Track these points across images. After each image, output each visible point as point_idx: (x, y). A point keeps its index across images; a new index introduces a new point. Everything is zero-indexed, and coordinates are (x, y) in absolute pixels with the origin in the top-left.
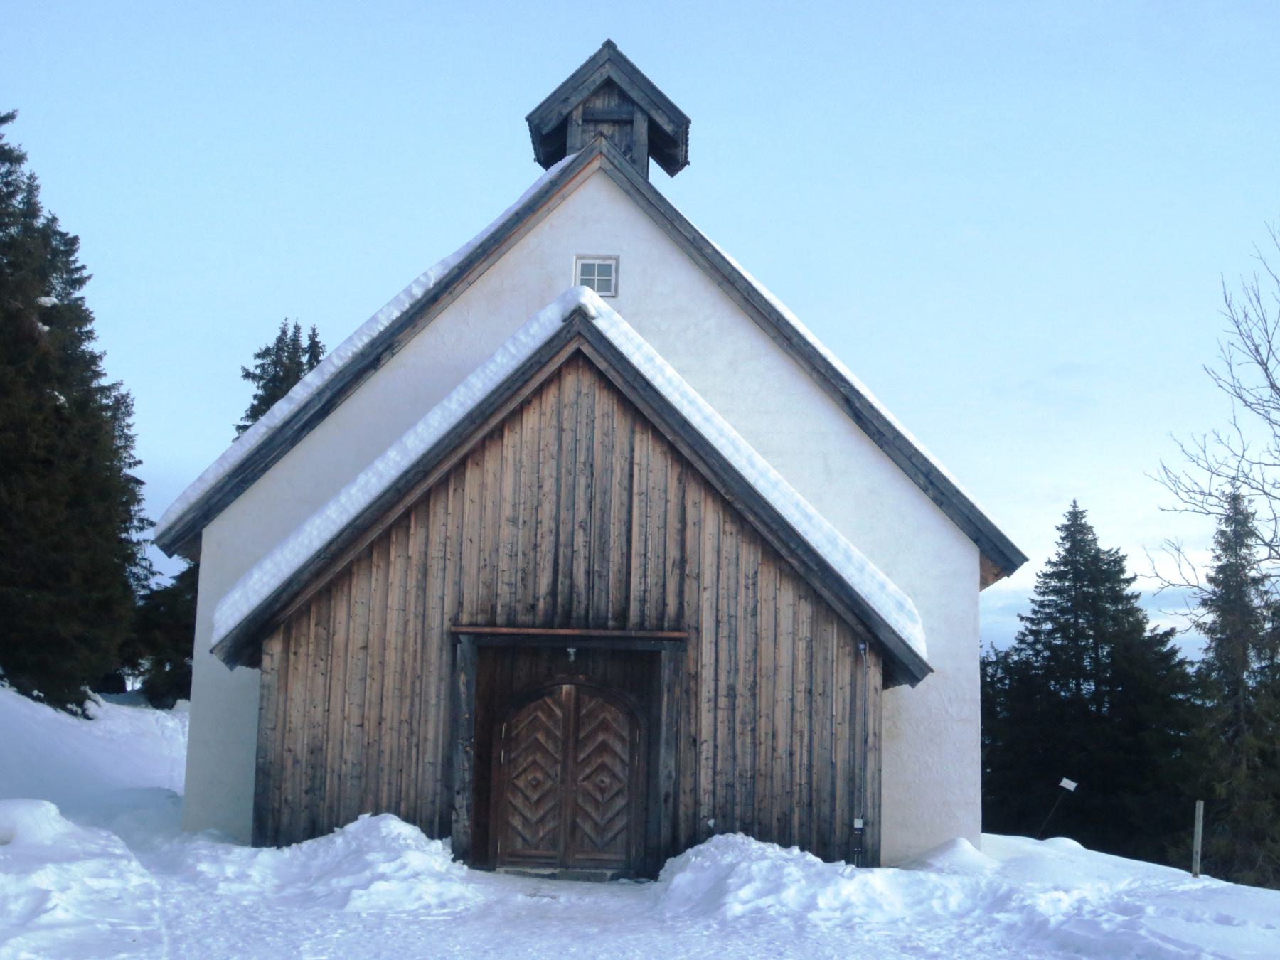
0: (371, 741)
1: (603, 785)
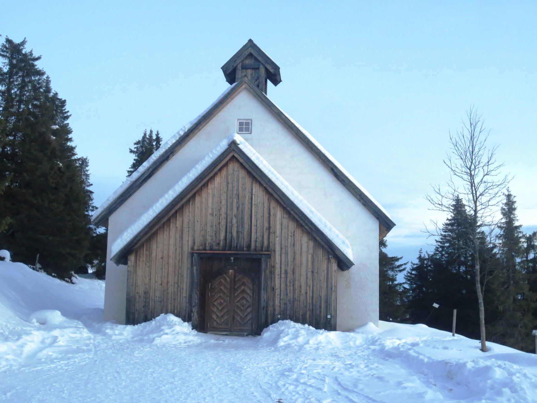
0: (165, 289)
1: (243, 304)
